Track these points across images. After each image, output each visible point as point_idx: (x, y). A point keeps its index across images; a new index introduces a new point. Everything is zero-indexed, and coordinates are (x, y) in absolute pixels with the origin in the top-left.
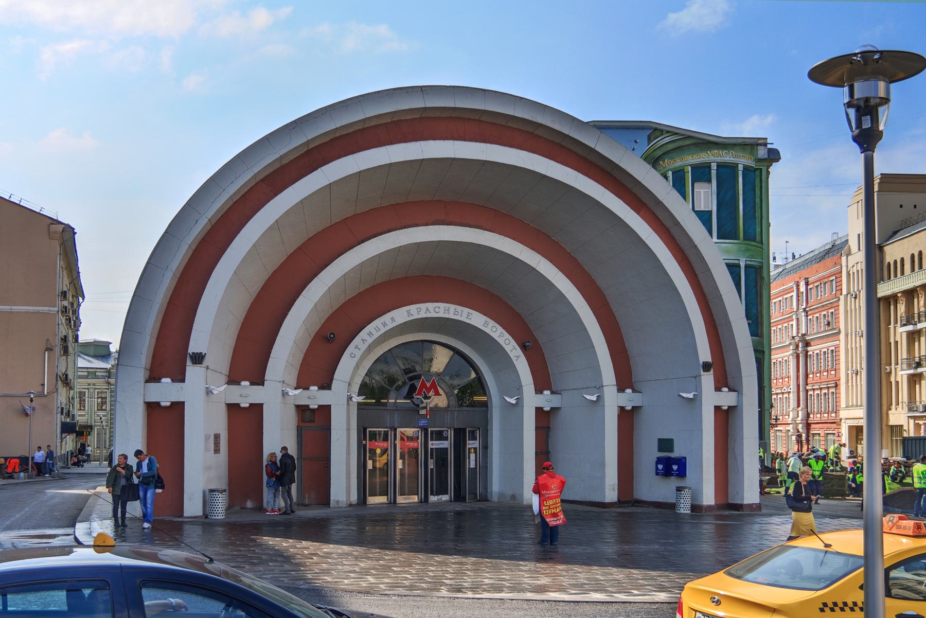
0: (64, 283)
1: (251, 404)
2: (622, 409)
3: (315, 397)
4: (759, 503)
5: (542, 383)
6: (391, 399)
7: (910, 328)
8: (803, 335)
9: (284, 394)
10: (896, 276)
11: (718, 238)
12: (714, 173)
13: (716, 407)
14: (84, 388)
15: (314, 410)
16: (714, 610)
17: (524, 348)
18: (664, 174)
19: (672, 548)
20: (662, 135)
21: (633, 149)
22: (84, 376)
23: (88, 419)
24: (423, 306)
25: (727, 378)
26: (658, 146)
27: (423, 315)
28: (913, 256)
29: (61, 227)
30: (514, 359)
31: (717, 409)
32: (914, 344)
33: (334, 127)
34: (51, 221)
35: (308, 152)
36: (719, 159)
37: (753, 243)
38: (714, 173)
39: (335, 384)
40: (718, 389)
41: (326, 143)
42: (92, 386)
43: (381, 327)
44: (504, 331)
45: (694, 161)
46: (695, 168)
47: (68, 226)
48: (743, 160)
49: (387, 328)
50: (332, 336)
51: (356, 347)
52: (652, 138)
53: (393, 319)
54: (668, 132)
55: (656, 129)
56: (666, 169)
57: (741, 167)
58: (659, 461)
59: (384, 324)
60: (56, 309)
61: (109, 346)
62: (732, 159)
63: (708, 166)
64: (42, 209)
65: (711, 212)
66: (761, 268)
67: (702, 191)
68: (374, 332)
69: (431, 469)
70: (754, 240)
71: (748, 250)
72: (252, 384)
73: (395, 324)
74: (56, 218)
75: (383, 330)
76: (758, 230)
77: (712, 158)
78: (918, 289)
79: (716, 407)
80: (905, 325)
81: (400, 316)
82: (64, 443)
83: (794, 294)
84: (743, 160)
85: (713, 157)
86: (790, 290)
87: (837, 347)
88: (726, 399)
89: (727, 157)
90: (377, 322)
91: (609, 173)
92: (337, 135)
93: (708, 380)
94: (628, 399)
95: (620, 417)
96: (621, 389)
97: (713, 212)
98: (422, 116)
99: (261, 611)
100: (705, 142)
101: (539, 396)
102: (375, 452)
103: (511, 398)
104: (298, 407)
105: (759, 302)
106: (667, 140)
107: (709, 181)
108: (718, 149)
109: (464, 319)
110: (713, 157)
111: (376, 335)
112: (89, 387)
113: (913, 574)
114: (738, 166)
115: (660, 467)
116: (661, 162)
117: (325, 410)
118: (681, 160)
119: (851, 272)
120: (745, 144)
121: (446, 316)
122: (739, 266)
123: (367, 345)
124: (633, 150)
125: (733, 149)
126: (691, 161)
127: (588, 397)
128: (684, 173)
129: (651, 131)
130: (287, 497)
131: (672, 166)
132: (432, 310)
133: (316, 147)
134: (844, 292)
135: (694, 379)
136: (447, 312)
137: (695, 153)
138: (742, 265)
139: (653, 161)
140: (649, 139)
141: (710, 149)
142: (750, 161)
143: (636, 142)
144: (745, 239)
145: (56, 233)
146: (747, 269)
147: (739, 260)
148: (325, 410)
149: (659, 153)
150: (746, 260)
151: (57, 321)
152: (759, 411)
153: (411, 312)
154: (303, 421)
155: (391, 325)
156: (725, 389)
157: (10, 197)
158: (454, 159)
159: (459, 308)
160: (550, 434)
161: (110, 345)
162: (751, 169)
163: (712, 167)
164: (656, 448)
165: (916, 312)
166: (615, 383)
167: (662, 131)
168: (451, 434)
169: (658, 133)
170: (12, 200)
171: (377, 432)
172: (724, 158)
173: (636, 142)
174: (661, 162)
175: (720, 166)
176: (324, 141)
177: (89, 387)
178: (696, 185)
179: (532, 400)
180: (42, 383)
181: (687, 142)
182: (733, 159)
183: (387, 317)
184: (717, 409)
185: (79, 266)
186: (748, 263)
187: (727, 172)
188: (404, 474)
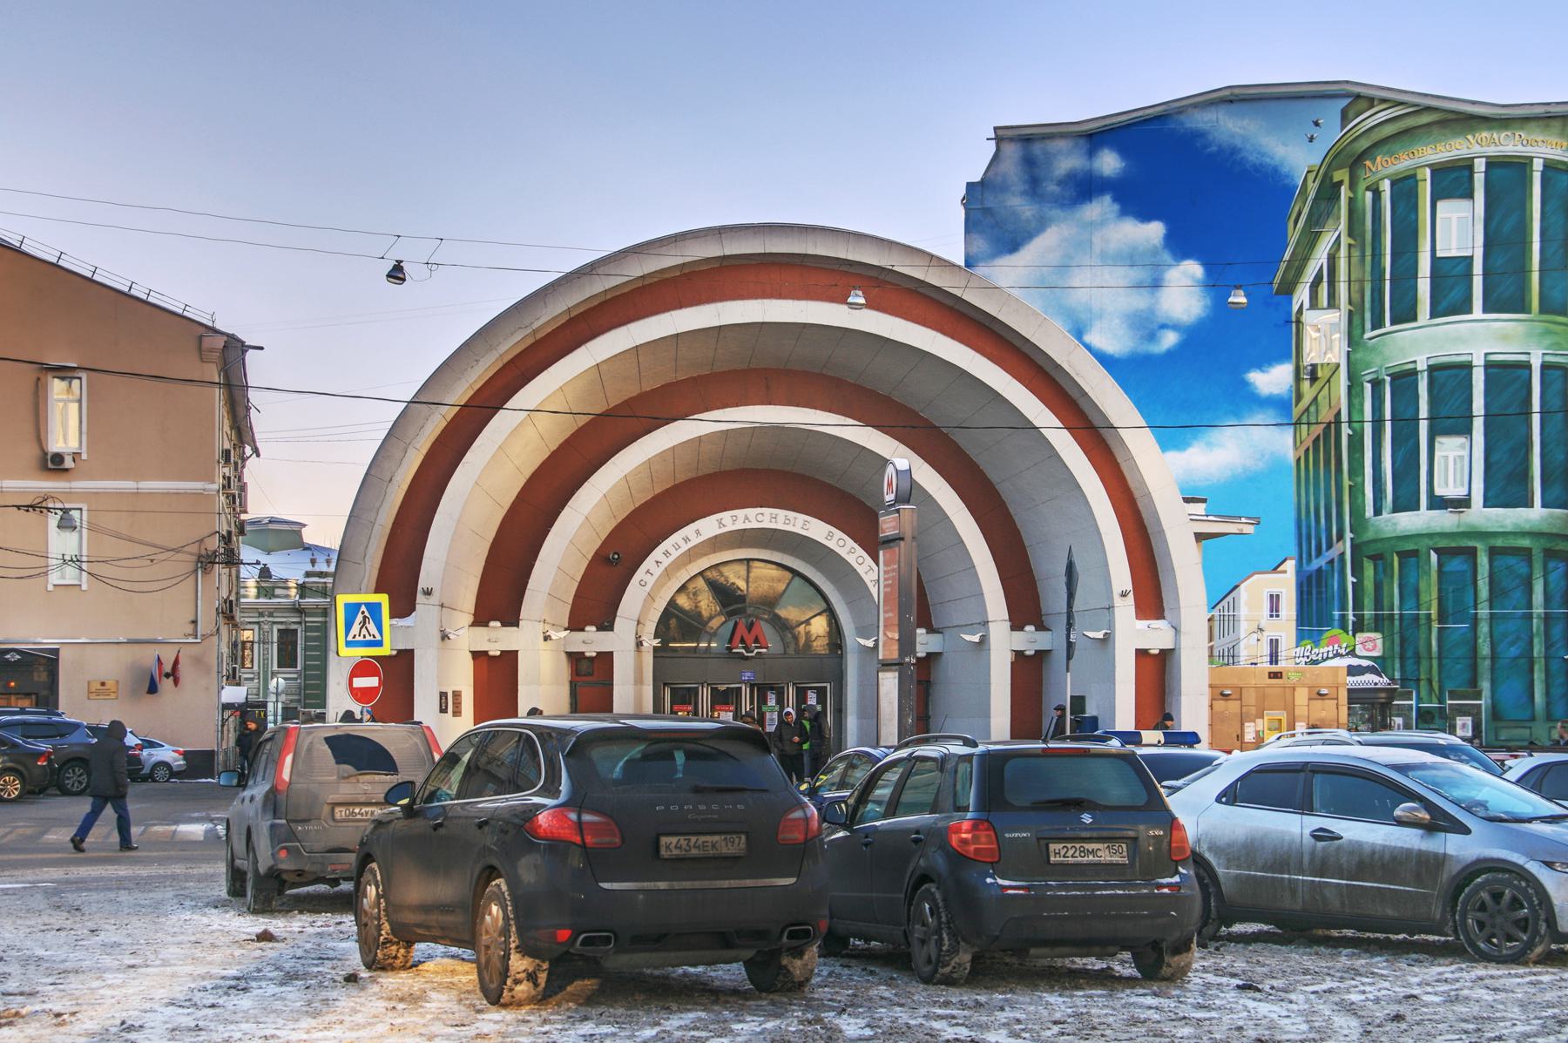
0: (223, 439)
1: (598, 653)
2: (1019, 655)
3: (591, 641)
6: (704, 642)
11: (1485, 311)
14: (250, 623)
15: (591, 659)
16: (889, 823)
18: (1375, 187)
20: (1372, 106)
21: (1311, 139)
23: (259, 689)
24: (740, 513)
26: (1363, 129)
27: (740, 526)
29: (220, 342)
31: (1141, 654)
33: (602, 289)
34: (202, 330)
35: (571, 321)
36: (1492, 151)
39: (619, 623)
41: (596, 307)
42: (266, 618)
43: (682, 543)
44: (856, 546)
45: (1438, 156)
46: (1438, 171)
47: (232, 337)
49: (690, 545)
50: (616, 556)
51: (648, 572)
52: (1351, 114)
53: (698, 533)
54: (1384, 101)
55: (1358, 97)
56: (1378, 176)
57: (1538, 165)
59: (686, 540)
60: (215, 487)
61: (300, 531)
62: (1520, 148)
63: (1467, 166)
64: (187, 308)
65: (1469, 260)
67: (1454, 216)
68: (672, 550)
71: (1548, 332)
72: (504, 625)
73: (701, 539)
74: (210, 324)
75: (685, 547)
77: (1476, 149)
81: (709, 527)
82: (225, 728)
84: (1543, 150)
85: (1478, 147)
88: (1155, 636)
89: (1508, 144)
90: (676, 537)
91: (988, 327)
92: (609, 297)
94: (1029, 640)
95: (1014, 666)
96: (1017, 625)
97: (1475, 258)
100: (1460, 116)
103: (868, 639)
104: (570, 655)
107: (1469, 195)
108: (1490, 129)
109: (797, 530)
110: (1478, 147)
111: (675, 554)
112: (262, 619)
114: (1532, 161)
116: (1368, 163)
117: (606, 658)
118: (1411, 156)
120: (1549, 117)
121: (773, 526)
122: (1527, 366)
123: (662, 567)
124: (1311, 141)
125: (1522, 129)
126: (1433, 157)
128: (1417, 182)
129: (1350, 100)
131: (1392, 170)
132: (752, 518)
133: (581, 313)
135: (1106, 611)
136: (774, 520)
137: (1440, 141)
138: (1536, 364)
139: (1351, 161)
140: (1345, 117)
141: (1472, 130)
142: (1559, 151)
143: (1317, 124)
144: (1543, 310)
145: (211, 350)
146: (1546, 371)
147: (1529, 354)
148: (606, 658)
149: (1364, 144)
150: (1544, 354)
151: (45, 641)
153: (723, 522)
154: (577, 674)
155: (695, 541)
157: (131, 288)
158: (763, 323)
159: (791, 514)
160: (931, 691)
161: (303, 530)
162: (1559, 166)
163: (1476, 166)
166: (1007, 618)
167: (1371, 101)
169: (1362, 104)
170: (133, 292)
172: (1501, 148)
173: (1317, 124)
174: (1368, 163)
175: (1493, 164)
176: (592, 305)
177: (262, 619)
178: (1441, 205)
180: (193, 618)
181: (1425, 119)
182: (1523, 149)
183: (689, 530)
184: (1141, 654)
186: (1548, 359)
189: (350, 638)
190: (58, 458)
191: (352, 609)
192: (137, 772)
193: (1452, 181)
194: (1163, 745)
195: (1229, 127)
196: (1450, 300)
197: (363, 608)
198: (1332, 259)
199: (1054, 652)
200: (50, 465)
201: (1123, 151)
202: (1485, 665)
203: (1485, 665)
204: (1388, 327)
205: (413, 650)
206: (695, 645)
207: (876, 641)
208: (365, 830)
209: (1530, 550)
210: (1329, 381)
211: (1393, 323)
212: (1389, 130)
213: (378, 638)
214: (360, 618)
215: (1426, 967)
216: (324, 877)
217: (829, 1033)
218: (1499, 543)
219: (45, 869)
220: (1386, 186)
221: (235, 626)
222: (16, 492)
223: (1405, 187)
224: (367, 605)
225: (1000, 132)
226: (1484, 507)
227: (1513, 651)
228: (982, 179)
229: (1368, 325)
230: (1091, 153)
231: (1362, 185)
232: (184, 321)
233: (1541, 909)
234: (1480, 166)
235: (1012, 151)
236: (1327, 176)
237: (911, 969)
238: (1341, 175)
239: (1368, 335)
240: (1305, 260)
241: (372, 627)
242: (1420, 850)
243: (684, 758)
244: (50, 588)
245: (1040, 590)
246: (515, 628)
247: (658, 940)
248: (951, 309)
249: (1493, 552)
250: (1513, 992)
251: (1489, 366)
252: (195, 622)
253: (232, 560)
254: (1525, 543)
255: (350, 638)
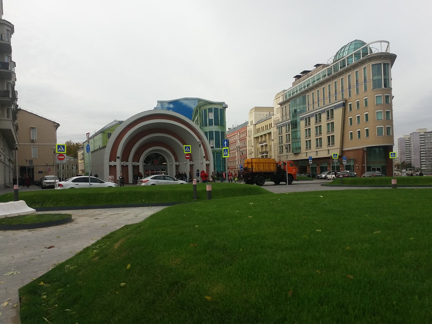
2: (190, 165)
3: (136, 164)
4: (265, 179)
5: (176, 160)
7: (261, 145)
8: (239, 146)
9: (143, 164)
10: (258, 128)
12: (213, 110)
13: (206, 164)
17: (173, 154)
19: (46, 256)
22: (422, 146)
25: (361, 41)
28: (270, 124)
30: (171, 156)
32: (344, 151)
36: (214, 107)
37: (222, 127)
38: (213, 110)
40: (206, 161)
46: (209, 109)
47: (58, 124)
48: (220, 107)
52: (199, 102)
57: (219, 109)
58: (197, 173)
65: (393, 152)
66: (224, 132)
67: (211, 114)
69: (16, 184)
70: (223, 126)
76: (223, 123)
77: (213, 107)
78: (267, 134)
79: (206, 164)
80: (260, 144)
81: (151, 149)
83: (237, 136)
85: (213, 107)
86: (236, 135)
87: (247, 149)
88: (208, 162)
89: (216, 106)
93: (205, 159)
96: (176, 162)
98: (59, 181)
99: (17, 140)
101: (190, 162)
102: (206, 282)
105: (216, 162)
106: (202, 102)
113: (393, 99)
115: (197, 174)
119: (275, 120)
127: (185, 163)
130: (42, 231)
131: (204, 109)
134: (248, 136)
138: (220, 132)
141: (212, 105)
144: (220, 125)
149: (200, 105)
151: (122, 216)
152: (122, 207)
156: (208, 161)
161: (18, 99)
164: (197, 171)
165: (263, 141)
168: (362, 176)
169: (357, 72)
171: (320, 145)
179: (175, 163)
180: (49, 171)
181: (207, 103)
185: (9, 202)
187: (216, 110)
188: (14, 110)
189: (185, 151)
190: (33, 140)
191: (224, 150)
192: (237, 181)
193: (210, 110)
194: (166, 171)
195: (182, 101)
196: (211, 124)
197: (226, 150)
198: (198, 119)
199: (180, 165)
200: (32, 141)
201: (173, 104)
202: (216, 166)
203: (216, 166)
204: (204, 127)
205: (139, 165)
206: (387, 80)
207: (390, 104)
208: (19, 316)
209: (220, 153)
210: (279, 97)
211: (205, 126)
212: (204, 104)
213: (64, 150)
214: (187, 148)
215: (195, 201)
216: (91, 173)
217: (225, 289)
218: (217, 152)
219: (74, 210)
220: (203, 110)
221: (346, 101)
222: (359, 149)
223: (205, 111)
224: (188, 147)
225: (158, 101)
226: (197, 170)
227: (219, 164)
228: (20, 109)
229: (202, 127)
230: (169, 105)
231: (201, 110)
232: (45, 120)
233: (279, 298)
234: (213, 109)
235: (160, 104)
236: (197, 109)
237: (168, 102)
238: (198, 109)
239: (202, 128)
240: (195, 119)
241: (188, 149)
242: (143, 221)
243: (280, 106)
244: (32, 158)
245: (95, 187)
246: (228, 112)
247: (95, 215)
248: (195, 100)
249: (216, 153)
250: (88, 220)
251: (215, 132)
252: (54, 163)
253: (170, 273)
254: (220, 152)
255: (185, 151)
